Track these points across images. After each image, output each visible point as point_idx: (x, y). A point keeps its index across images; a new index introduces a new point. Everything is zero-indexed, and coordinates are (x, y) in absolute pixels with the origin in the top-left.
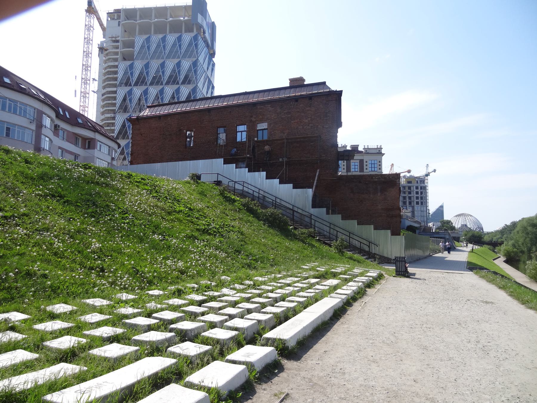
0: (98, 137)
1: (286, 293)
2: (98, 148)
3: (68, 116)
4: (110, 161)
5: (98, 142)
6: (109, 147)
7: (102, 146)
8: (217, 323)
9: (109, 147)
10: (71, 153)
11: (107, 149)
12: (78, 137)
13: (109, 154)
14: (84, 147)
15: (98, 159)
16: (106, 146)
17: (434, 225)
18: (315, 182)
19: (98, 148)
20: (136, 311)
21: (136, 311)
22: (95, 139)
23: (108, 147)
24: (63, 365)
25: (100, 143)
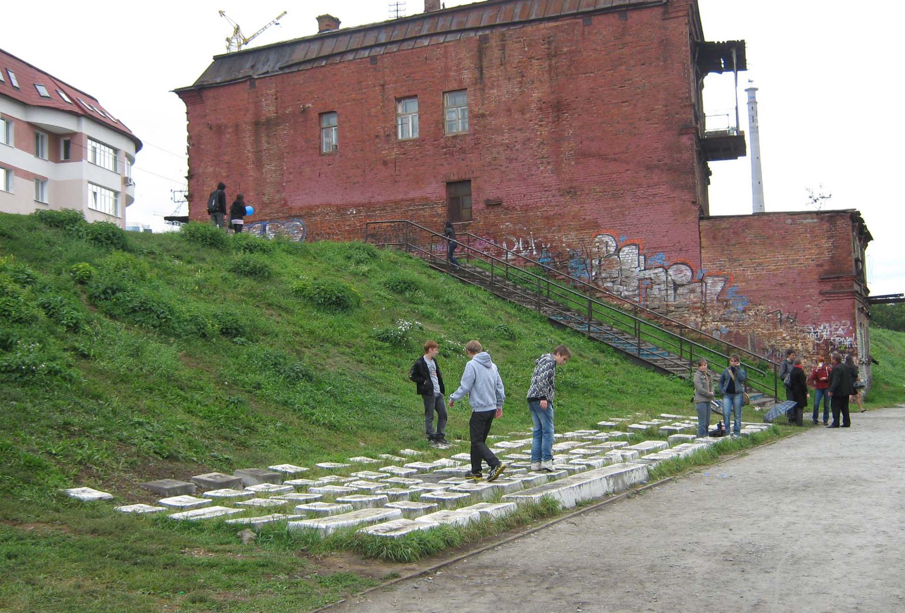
0: (86, 128)
1: (334, 491)
2: (90, 158)
3: (15, 83)
4: (118, 187)
5: (89, 141)
6: (116, 151)
7: (98, 151)
8: (785, 398)
9: (116, 151)
10: (27, 175)
11: (111, 156)
12: (41, 133)
13: (115, 171)
14: (55, 158)
15: (90, 185)
16: (107, 149)
17: (772, 313)
18: (735, 61)
19: (90, 158)
20: (300, 469)
21: (300, 469)
22: (81, 134)
23: (111, 151)
24: (218, 508)
25: (94, 144)
